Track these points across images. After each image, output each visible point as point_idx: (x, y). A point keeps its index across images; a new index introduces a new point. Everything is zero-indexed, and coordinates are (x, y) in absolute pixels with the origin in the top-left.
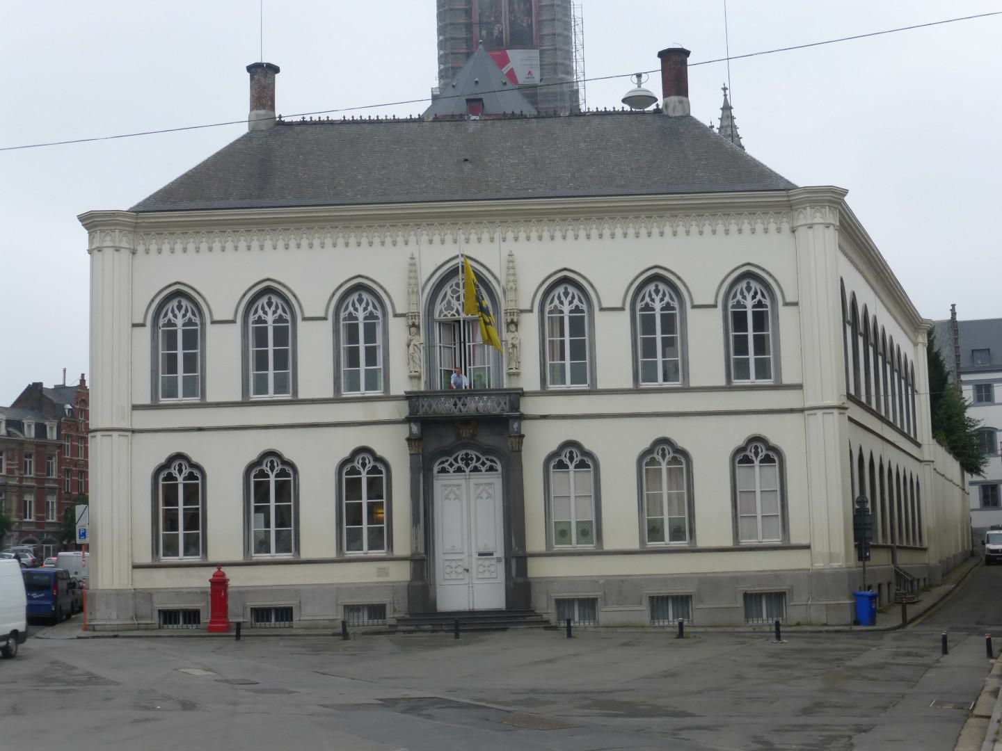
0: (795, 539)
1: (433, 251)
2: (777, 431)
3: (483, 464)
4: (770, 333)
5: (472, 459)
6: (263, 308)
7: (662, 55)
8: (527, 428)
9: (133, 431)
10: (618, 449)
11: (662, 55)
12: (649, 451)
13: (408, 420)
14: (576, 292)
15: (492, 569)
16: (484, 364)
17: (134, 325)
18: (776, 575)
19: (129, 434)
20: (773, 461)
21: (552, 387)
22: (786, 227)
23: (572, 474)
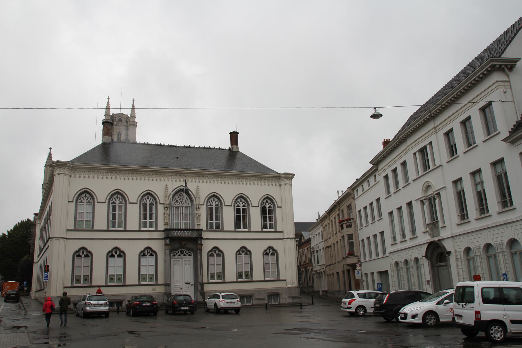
0: (282, 278)
1: (175, 183)
2: (276, 245)
7: (231, 133)
8: (204, 242)
9: (67, 239)
10: (230, 249)
11: (231, 133)
12: (239, 251)
13: (164, 239)
14: (121, 197)
17: (69, 202)
18: (277, 289)
21: (142, 229)
22: (278, 184)
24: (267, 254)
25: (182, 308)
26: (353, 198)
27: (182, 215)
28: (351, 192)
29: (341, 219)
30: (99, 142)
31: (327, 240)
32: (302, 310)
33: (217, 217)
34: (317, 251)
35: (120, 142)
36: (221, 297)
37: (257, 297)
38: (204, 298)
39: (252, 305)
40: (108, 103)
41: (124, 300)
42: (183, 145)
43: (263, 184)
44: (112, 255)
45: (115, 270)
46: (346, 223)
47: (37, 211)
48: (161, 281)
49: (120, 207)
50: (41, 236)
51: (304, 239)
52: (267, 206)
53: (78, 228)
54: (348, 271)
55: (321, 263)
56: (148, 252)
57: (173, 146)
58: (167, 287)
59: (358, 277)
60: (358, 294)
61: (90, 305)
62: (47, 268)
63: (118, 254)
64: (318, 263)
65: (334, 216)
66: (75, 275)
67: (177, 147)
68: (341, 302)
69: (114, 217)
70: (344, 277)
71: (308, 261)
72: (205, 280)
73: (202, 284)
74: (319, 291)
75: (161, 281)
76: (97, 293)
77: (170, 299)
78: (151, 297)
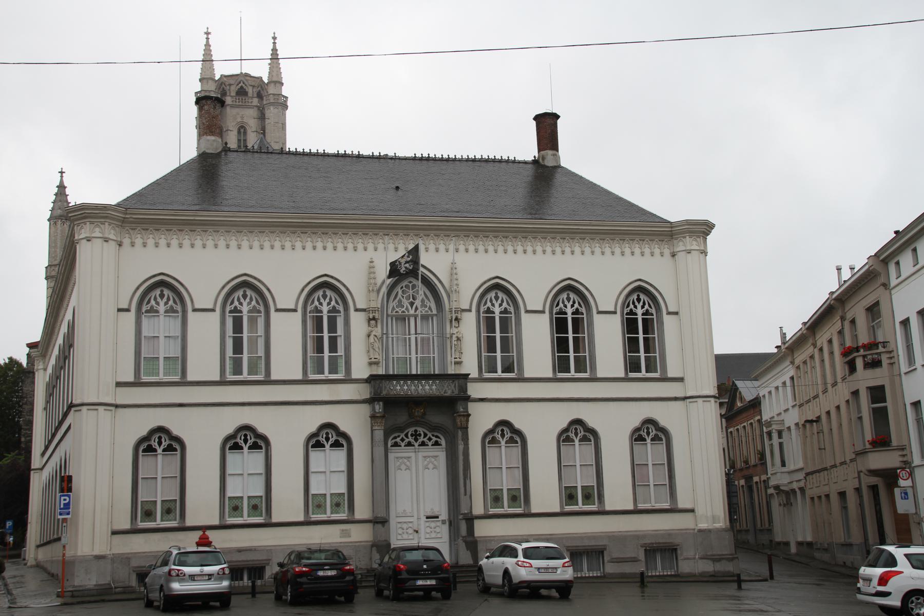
2: (665, 415)
3: (430, 439)
4: (656, 336)
5: (420, 435)
6: (239, 299)
8: (472, 408)
9: (117, 406)
10: (541, 427)
12: (566, 430)
13: (370, 401)
14: (254, 295)
15: (438, 530)
16: (429, 353)
17: (119, 310)
18: (669, 533)
19: (113, 408)
20: (261, 448)
22: (667, 252)
23: (160, 457)
24: (641, 439)
25: (420, 583)
26: (885, 286)
27: (413, 338)
28: (879, 267)
29: (848, 343)
30: (190, 152)
31: (808, 401)
32: (742, 593)
33: (505, 342)
34: (780, 433)
35: (247, 151)
36: (520, 553)
37: (615, 555)
38: (476, 558)
39: (604, 577)
40: (208, 45)
41: (268, 561)
42: (410, 154)
43: (627, 251)
44: (236, 447)
45: (245, 484)
46: (864, 356)
47: (36, 337)
48: (362, 510)
49: (253, 321)
50: (47, 402)
51: (741, 399)
52: (639, 311)
53: (145, 379)
54: (874, 489)
55: (791, 466)
56: (327, 437)
57: (386, 157)
58: (380, 526)
59: (903, 507)
60: (906, 555)
61: (181, 577)
62: (66, 483)
63: (250, 442)
64: (783, 464)
65: (827, 336)
66: (140, 499)
67: (395, 158)
68: (856, 577)
69: (238, 347)
70: (861, 505)
71: (753, 460)
72: (478, 509)
73: (470, 520)
74: (787, 544)
75: (362, 510)
76: (198, 544)
77: (386, 559)
78: (337, 553)
